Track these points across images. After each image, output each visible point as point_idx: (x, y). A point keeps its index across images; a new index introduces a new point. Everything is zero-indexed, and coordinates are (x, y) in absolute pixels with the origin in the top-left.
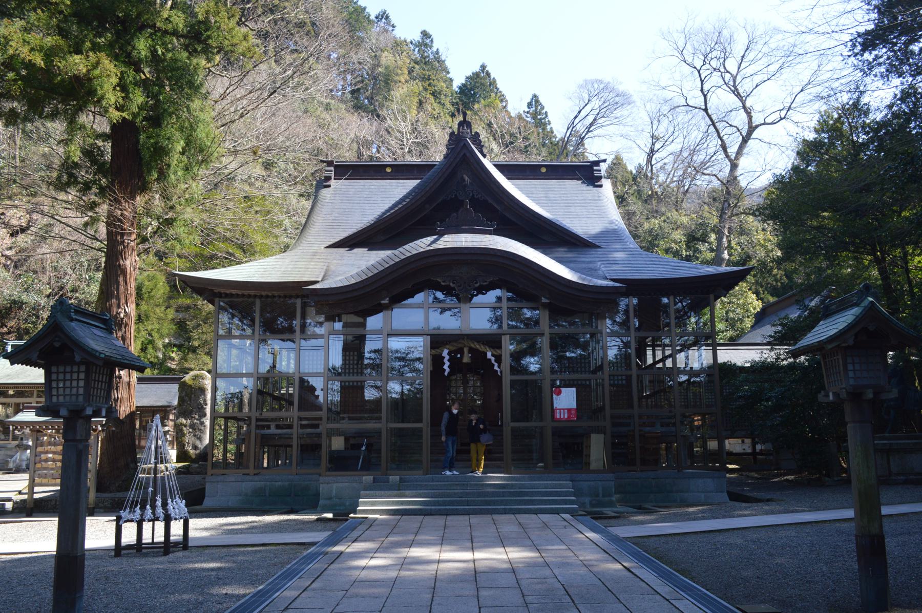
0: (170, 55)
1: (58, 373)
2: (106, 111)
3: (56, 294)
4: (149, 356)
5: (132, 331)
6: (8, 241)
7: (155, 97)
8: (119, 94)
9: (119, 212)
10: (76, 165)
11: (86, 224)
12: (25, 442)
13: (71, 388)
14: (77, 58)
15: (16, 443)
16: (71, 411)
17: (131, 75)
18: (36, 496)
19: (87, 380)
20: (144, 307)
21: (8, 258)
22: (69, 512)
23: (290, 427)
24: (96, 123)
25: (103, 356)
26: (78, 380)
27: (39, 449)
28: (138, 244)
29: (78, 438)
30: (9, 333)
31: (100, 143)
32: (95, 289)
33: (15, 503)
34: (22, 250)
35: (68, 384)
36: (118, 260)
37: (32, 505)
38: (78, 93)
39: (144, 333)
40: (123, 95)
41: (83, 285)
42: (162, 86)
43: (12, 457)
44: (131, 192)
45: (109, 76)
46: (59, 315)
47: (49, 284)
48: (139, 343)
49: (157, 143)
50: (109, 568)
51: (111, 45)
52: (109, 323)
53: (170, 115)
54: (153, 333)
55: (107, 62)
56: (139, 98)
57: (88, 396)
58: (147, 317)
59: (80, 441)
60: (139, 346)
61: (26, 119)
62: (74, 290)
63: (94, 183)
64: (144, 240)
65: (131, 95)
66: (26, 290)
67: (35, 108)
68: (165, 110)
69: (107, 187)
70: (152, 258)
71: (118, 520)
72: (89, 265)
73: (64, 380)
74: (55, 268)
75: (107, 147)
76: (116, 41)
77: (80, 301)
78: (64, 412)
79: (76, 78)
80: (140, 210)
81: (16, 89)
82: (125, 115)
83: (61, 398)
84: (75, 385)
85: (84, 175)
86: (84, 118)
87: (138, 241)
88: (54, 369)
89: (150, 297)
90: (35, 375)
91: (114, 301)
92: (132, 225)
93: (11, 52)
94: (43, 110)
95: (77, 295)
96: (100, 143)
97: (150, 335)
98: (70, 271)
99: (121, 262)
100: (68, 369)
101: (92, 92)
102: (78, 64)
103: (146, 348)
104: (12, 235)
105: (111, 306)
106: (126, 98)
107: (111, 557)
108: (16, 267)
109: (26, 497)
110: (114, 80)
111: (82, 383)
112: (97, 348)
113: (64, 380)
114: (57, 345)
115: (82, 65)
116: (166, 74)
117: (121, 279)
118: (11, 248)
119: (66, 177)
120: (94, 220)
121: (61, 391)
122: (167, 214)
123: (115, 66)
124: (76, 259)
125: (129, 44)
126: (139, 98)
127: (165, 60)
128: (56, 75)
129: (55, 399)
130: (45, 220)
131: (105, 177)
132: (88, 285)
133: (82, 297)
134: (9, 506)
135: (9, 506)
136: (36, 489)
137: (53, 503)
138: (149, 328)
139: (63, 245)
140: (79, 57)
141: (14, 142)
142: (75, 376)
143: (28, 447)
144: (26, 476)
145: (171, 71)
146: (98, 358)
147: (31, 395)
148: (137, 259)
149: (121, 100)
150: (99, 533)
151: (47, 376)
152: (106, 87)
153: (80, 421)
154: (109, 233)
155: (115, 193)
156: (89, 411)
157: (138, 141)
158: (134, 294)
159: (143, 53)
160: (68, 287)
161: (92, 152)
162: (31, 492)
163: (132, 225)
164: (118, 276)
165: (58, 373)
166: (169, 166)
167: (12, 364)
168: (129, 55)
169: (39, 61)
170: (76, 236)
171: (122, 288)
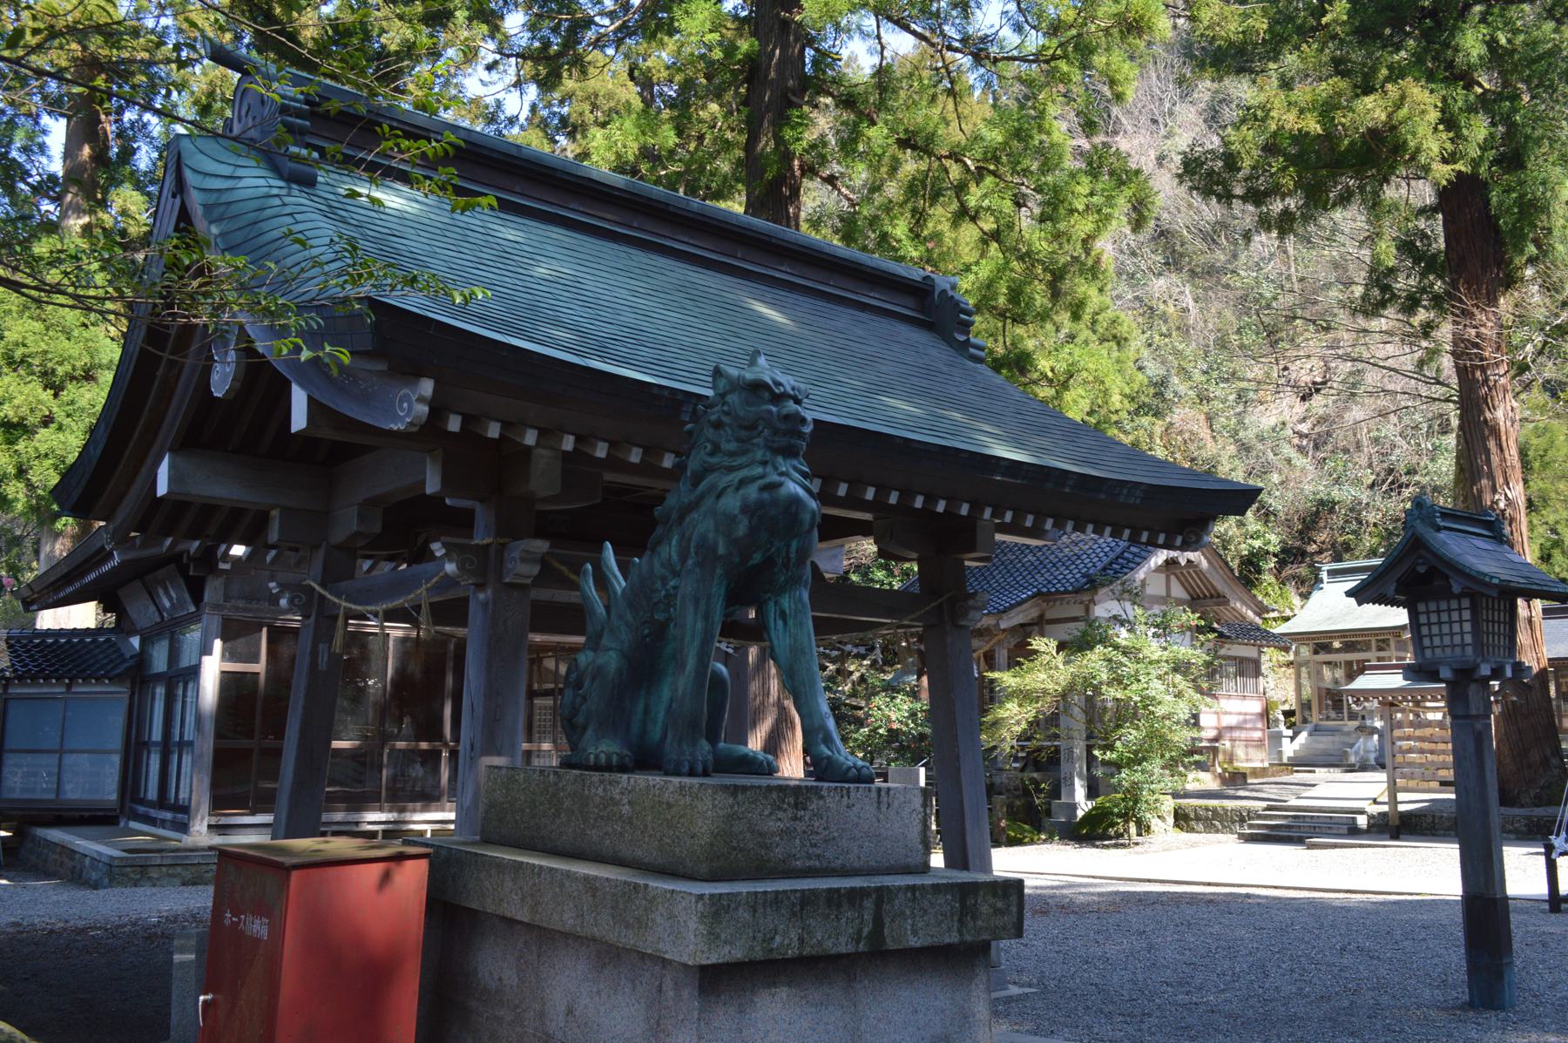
0: (1521, 37)
1: (1428, 613)
2: (1427, 169)
3: (1384, 482)
4: (1557, 569)
5: (1524, 529)
6: (1300, 408)
7: (1507, 120)
8: (1444, 136)
9: (1473, 332)
10: (1391, 271)
11: (1421, 363)
12: (1368, 723)
13: (1452, 634)
14: (1369, 101)
15: (1356, 723)
16: (1456, 671)
17: (1459, 96)
18: (1402, 808)
19: (1475, 621)
20: (1537, 484)
21: (1301, 435)
22: (1475, 831)
23: (1332, 573)
24: (1411, 193)
25: (1495, 581)
26: (1461, 621)
27: (1397, 733)
28: (1513, 378)
29: (1473, 712)
30: (1320, 552)
31: (1422, 224)
32: (1446, 466)
33: (1371, 817)
34: (1322, 420)
35: (1446, 629)
36: (1483, 412)
37: (1397, 822)
38: (1381, 153)
39: (1541, 530)
40: (1451, 135)
41: (1425, 461)
42: (1515, 97)
43: (1352, 746)
44: (1488, 294)
45: (1423, 112)
46: (1418, 525)
47: (1370, 466)
48: (1536, 548)
49: (1522, 196)
50: (1546, 929)
51: (1418, 59)
52: (1494, 528)
53: (1538, 142)
54: (1560, 528)
55: (1416, 90)
56: (1479, 129)
57: (1478, 645)
58: (1545, 500)
59: (1477, 717)
60: (1537, 554)
61: (1307, 218)
62: (1411, 472)
63: (1423, 290)
64: (1523, 368)
65: (1465, 132)
66: (1337, 481)
67: (1317, 198)
68: (1528, 137)
69: (1447, 293)
70: (1537, 396)
71: (1549, 849)
72: (1430, 427)
73: (1440, 623)
74: (1376, 441)
75: (1436, 227)
76: (1426, 50)
77: (1423, 488)
78: (1445, 673)
79: (1373, 133)
80: (1508, 319)
81: (1287, 182)
82: (1460, 167)
83: (1438, 651)
84: (1457, 630)
85: (1404, 283)
86: (1390, 193)
87: (1512, 372)
88: (1421, 607)
89: (1545, 466)
90: (1397, 616)
91: (1484, 482)
92: (1498, 349)
93: (1273, 127)
94: (1328, 198)
95: (1417, 478)
96: (1422, 224)
97: (1554, 531)
98: (1399, 441)
99: (1488, 415)
100: (1443, 605)
101: (1399, 147)
102: (1372, 110)
103: (1549, 556)
104: (1303, 399)
105: (1480, 491)
106: (1458, 137)
107: (1543, 912)
108: (1316, 447)
109: (1385, 808)
110: (1433, 116)
111: (1467, 627)
112: (1485, 569)
113: (1440, 623)
114: (1422, 569)
115: (1378, 111)
116: (1520, 73)
117: (1492, 444)
118: (1304, 420)
119: (1380, 293)
120: (1433, 354)
121: (1437, 641)
122: (1557, 316)
123: (1432, 92)
124: (1407, 420)
125: (1448, 46)
126: (1479, 129)
127: (1514, 50)
128: (1341, 139)
129: (1428, 653)
130: (1348, 366)
131: (1440, 277)
132: (1432, 460)
133: (1425, 480)
134: (1362, 821)
135: (1362, 821)
136: (1401, 796)
137: (1430, 820)
138: (1551, 519)
139: (1383, 402)
140: (1372, 97)
141: (1285, 252)
142: (1455, 616)
143: (1374, 730)
144: (1382, 776)
145: (1528, 66)
146: (1489, 585)
147: (1366, 647)
148: (1515, 404)
149: (1449, 146)
150: (1523, 872)
151: (1413, 615)
152: (1421, 131)
153: (1473, 687)
154: (1462, 372)
155: (1461, 301)
156: (1485, 670)
157: (1488, 202)
158: (1518, 465)
159: (1475, 53)
160: (1402, 468)
161: (1412, 243)
162: (1394, 801)
163: (1498, 349)
164: (1484, 440)
165: (1428, 613)
166: (1550, 230)
167: (1360, 604)
168: (1450, 65)
169: (1313, 126)
170: (1398, 384)
171: (1495, 459)
